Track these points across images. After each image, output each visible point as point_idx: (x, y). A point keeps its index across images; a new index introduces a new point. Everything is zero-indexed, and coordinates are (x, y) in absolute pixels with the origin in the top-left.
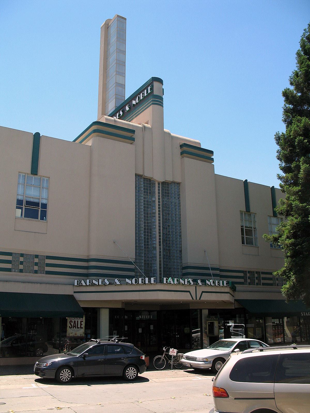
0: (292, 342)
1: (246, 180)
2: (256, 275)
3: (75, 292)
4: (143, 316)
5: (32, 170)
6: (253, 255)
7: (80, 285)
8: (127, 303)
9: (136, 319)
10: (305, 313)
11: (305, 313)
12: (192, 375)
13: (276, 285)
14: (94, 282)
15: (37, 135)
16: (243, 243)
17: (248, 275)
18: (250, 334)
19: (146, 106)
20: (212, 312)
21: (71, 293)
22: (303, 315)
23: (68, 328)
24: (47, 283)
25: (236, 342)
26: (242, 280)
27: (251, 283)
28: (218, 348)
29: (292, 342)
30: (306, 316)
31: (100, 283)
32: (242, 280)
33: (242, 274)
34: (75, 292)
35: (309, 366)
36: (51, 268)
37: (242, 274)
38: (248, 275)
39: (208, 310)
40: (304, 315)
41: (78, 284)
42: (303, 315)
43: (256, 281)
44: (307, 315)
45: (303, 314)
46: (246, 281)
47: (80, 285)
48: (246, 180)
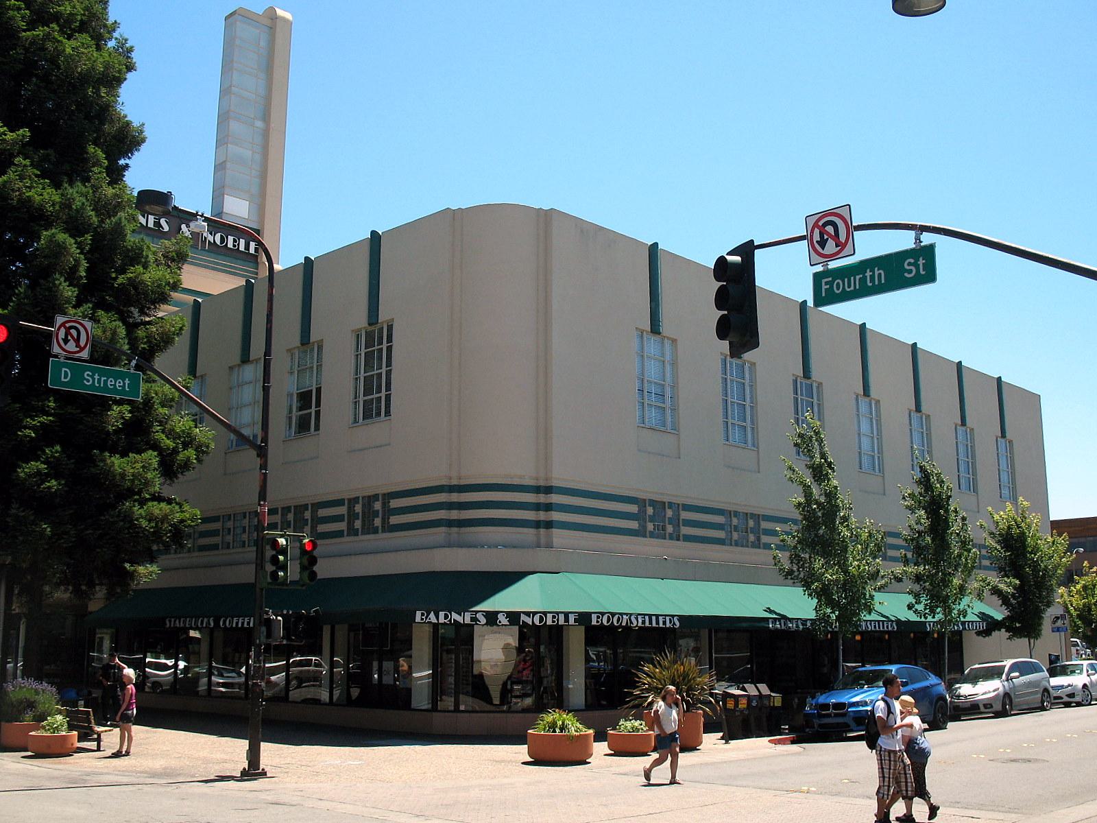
0: (584, 708)
1: (656, 245)
2: (669, 513)
4: (879, 628)
5: (215, 193)
6: (649, 453)
10: (175, 621)
11: (175, 621)
13: (731, 545)
15: (654, 249)
17: (650, 511)
18: (1033, 657)
22: (170, 624)
26: (634, 525)
27: (660, 534)
28: (874, 685)
29: (584, 708)
30: (176, 627)
33: (633, 509)
35: (321, 822)
36: (492, 482)
37: (633, 509)
38: (650, 511)
39: (254, 582)
40: (172, 626)
42: (170, 624)
43: (670, 529)
44: (178, 626)
45: (170, 621)
48: (656, 245)
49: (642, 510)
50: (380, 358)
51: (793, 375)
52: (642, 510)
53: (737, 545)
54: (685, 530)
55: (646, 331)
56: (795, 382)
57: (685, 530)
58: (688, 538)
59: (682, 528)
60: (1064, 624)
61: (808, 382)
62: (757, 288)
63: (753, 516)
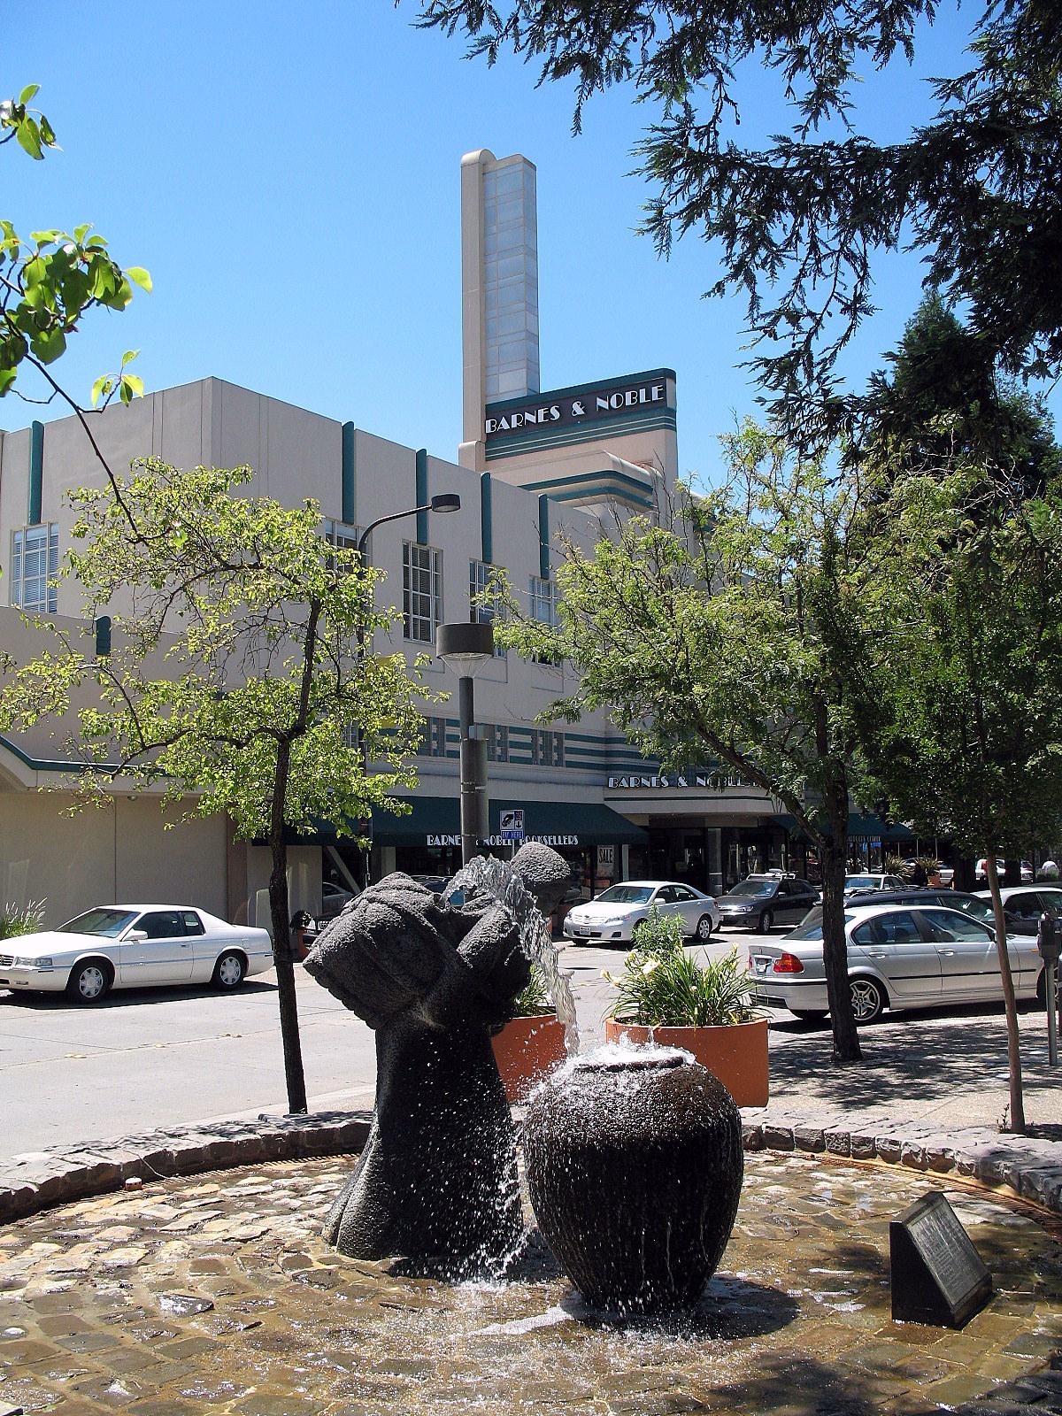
1: (351, 424)
3: (606, 799)
4: (557, 842)
7: (617, 787)
8: (654, 818)
9: (382, 848)
12: (607, 954)
14: (643, 781)
16: (407, 635)
19: (639, 425)
20: (728, 834)
21: (601, 801)
23: (598, 863)
24: (517, 781)
25: (138, 913)
27: (546, 762)
31: (654, 785)
32: (528, 754)
33: (527, 739)
34: (606, 799)
37: (527, 739)
38: (540, 741)
41: (615, 785)
43: (499, 751)
46: (535, 754)
47: (617, 787)
48: (351, 424)
49: (535, 740)
50: (43, 563)
51: (530, 575)
52: (535, 740)
53: (435, 755)
54: (568, 757)
55: (338, 521)
56: (473, 566)
57: (568, 757)
58: (570, 764)
59: (447, 743)
60: (519, 826)
61: (546, 582)
62: (492, 481)
63: (500, 728)
